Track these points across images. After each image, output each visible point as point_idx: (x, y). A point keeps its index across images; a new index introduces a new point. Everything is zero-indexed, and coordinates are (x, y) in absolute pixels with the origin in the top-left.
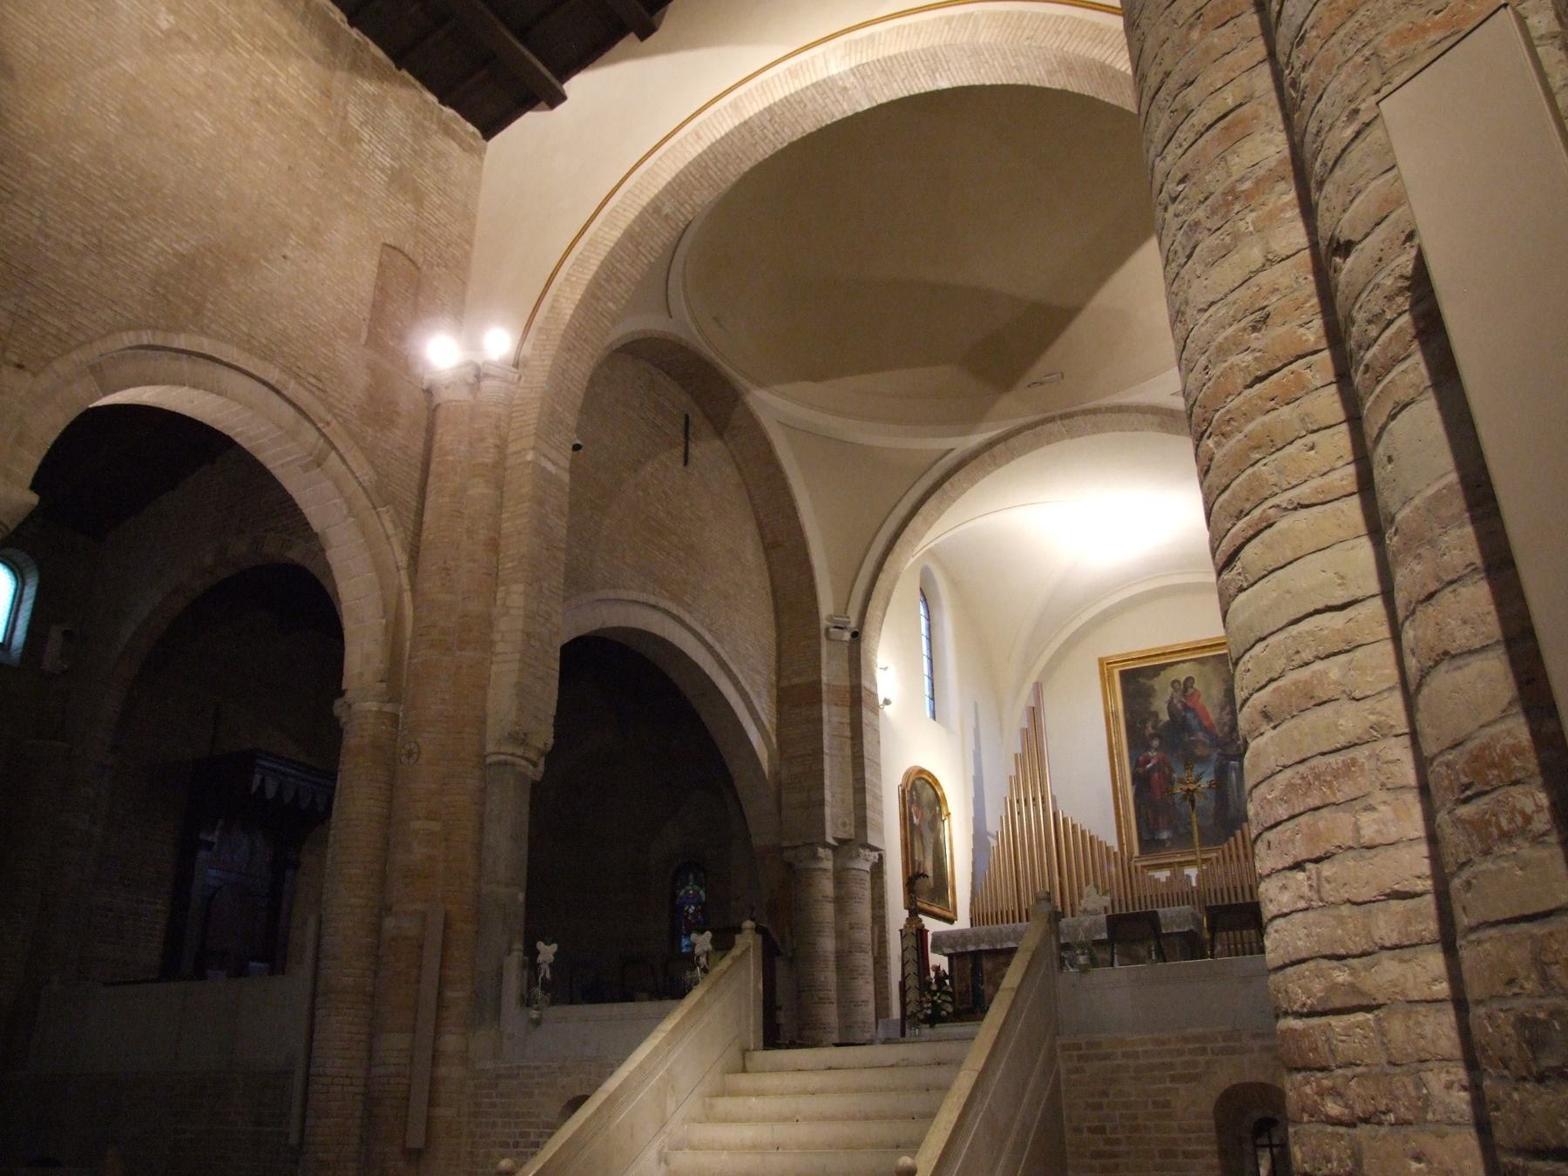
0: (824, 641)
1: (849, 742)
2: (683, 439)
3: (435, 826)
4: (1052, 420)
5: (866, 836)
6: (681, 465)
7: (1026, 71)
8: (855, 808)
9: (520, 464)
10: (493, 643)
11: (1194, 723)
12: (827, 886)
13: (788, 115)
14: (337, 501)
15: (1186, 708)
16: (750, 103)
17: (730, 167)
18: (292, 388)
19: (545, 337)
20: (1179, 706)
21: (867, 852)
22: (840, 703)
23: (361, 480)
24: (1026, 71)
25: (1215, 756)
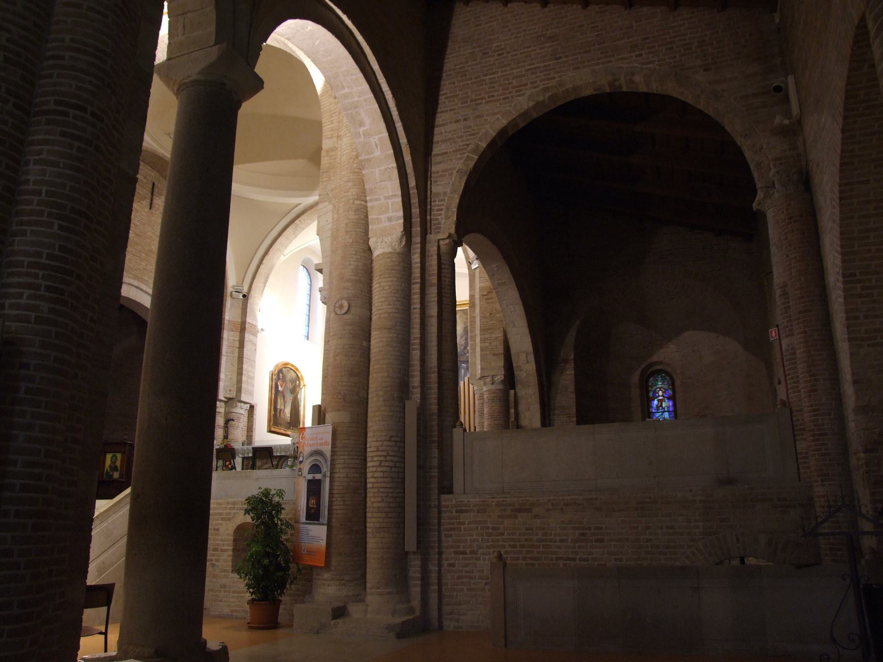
1: (237, 349)
2: (150, 195)
5: (241, 396)
6: (147, 209)
8: (237, 383)
21: (242, 404)
22: (234, 330)
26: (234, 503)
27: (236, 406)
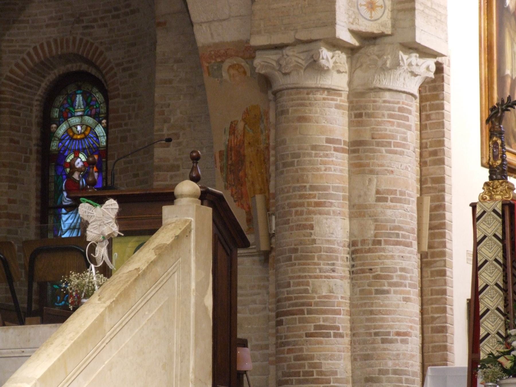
5: (413, 27)
21: (414, 58)
27: (397, 65)
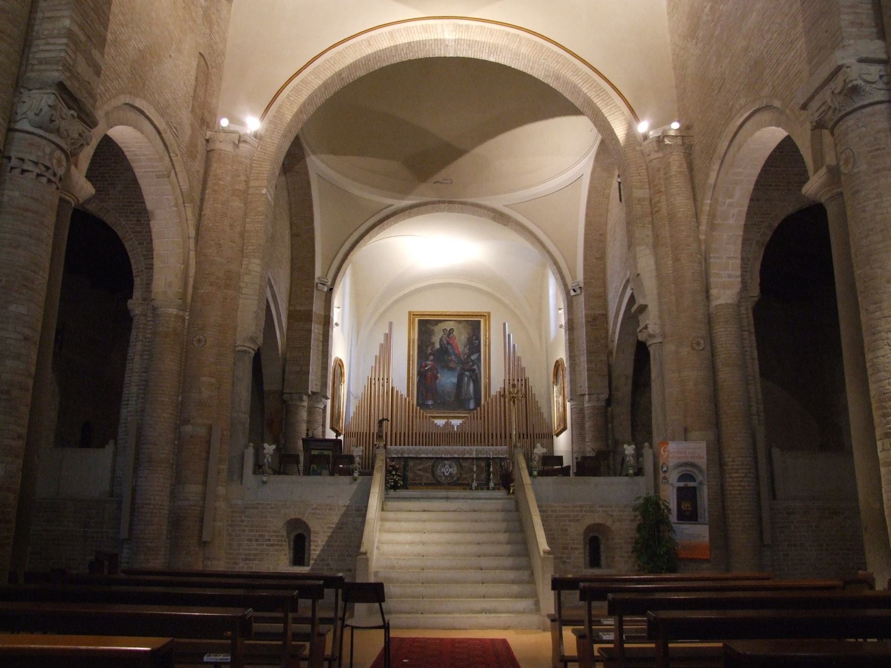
0: (315, 289)
3: (213, 380)
4: (444, 202)
7: (535, 70)
9: (257, 194)
10: (240, 288)
11: (451, 351)
12: (304, 415)
13: (416, 48)
14: (170, 197)
15: (448, 343)
16: (400, 37)
17: (378, 63)
18: (168, 136)
19: (274, 126)
20: (445, 342)
23: (182, 187)
24: (535, 70)
25: (459, 368)
26: (581, 506)
